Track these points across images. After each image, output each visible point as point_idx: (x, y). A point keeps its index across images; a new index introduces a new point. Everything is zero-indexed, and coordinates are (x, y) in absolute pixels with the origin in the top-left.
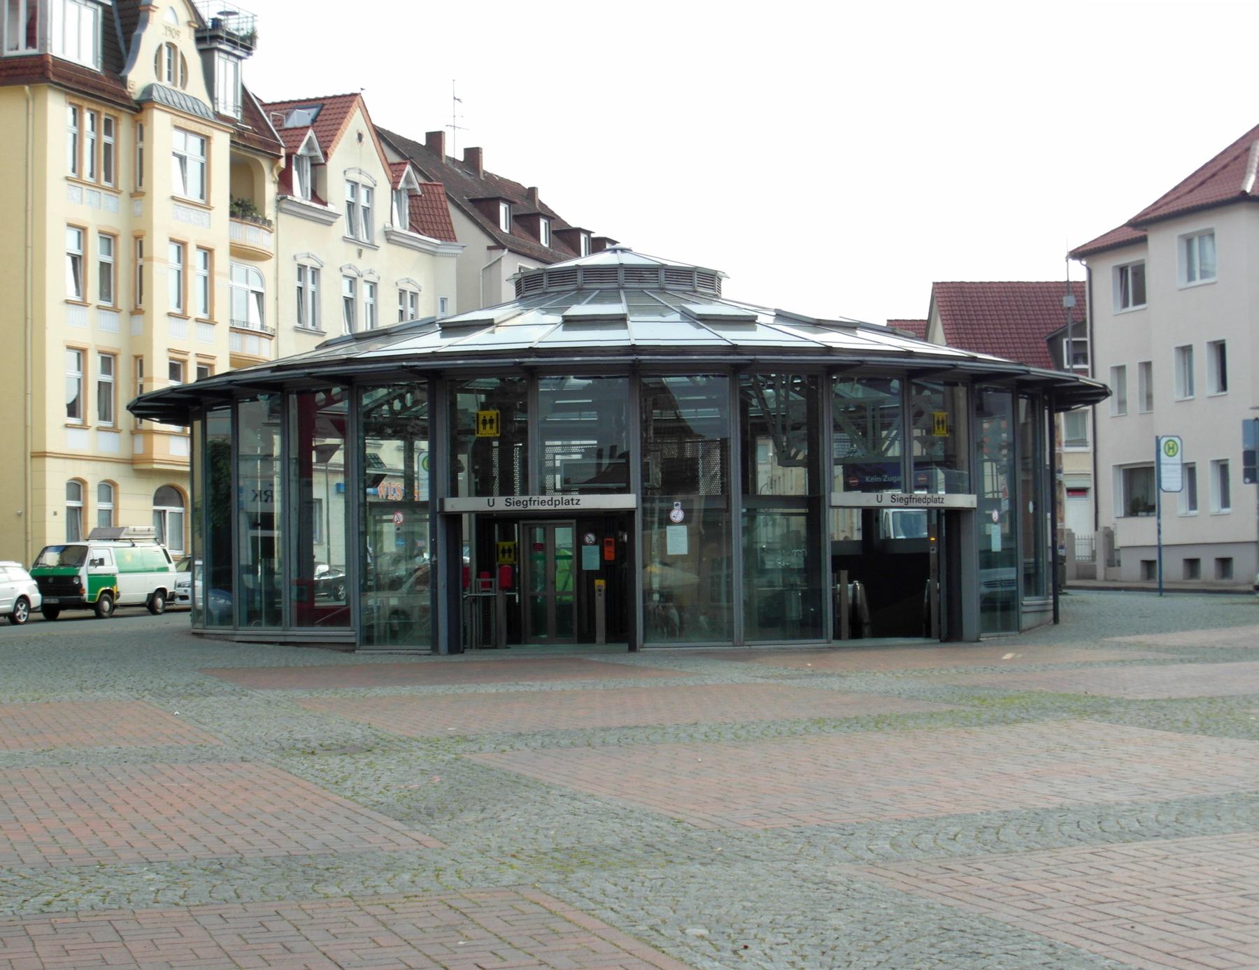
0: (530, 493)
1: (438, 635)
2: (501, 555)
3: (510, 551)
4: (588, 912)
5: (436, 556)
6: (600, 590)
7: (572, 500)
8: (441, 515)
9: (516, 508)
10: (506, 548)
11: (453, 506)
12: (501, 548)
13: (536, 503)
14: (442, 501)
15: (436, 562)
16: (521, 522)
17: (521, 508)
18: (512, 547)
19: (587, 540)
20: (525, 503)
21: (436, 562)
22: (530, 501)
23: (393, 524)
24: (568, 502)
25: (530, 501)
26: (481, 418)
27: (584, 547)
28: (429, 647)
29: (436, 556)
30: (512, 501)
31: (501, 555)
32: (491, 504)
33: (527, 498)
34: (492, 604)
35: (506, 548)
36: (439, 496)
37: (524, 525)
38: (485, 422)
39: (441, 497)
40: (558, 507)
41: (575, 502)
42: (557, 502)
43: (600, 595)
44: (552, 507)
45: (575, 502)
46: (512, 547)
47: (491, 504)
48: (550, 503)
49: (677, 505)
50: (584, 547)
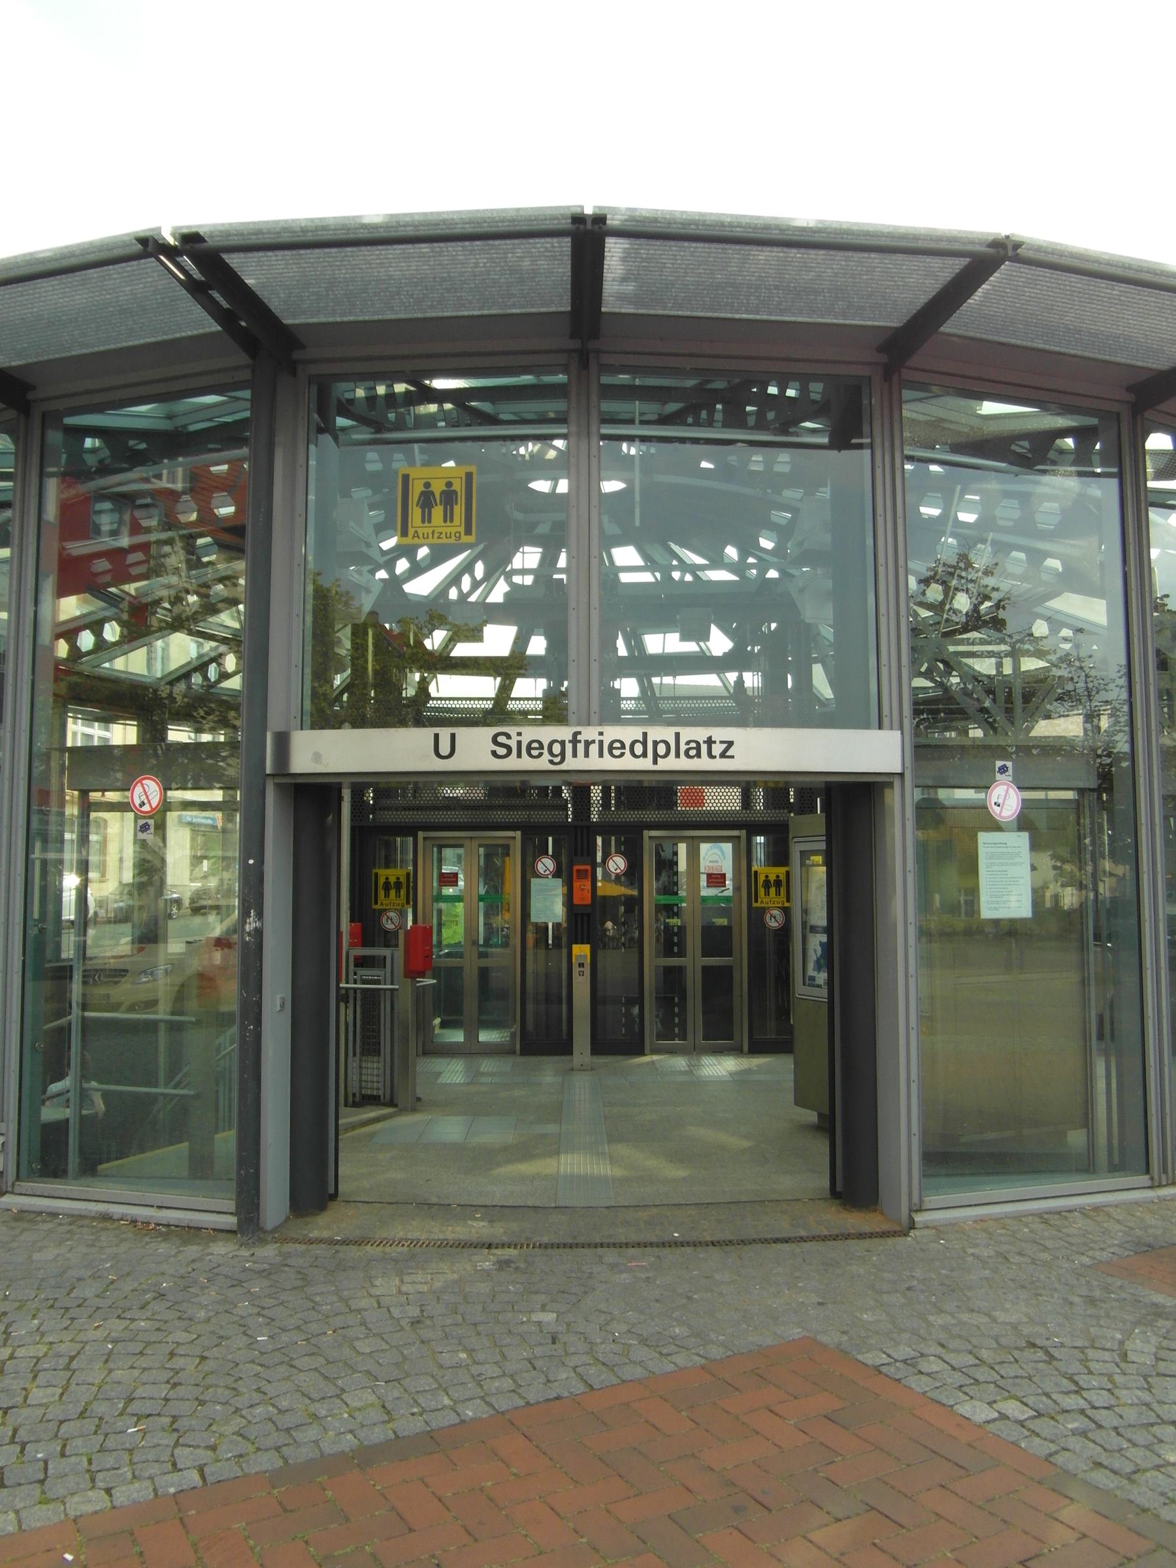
0: (572, 717)
1: (263, 863)
2: (382, 893)
3: (398, 885)
4: (22, 296)
5: (260, 916)
6: (581, 965)
7: (710, 742)
8: (278, 786)
9: (526, 763)
10: (392, 880)
11: (317, 757)
12: (382, 880)
13: (594, 748)
14: (283, 742)
15: (259, 933)
16: (421, 834)
17: (543, 763)
18: (403, 880)
19: (540, 868)
20: (557, 749)
21: (259, 933)
22: (575, 741)
23: (130, 816)
24: (695, 750)
25: (575, 741)
26: (417, 489)
27: (534, 881)
28: (231, 1206)
29: (260, 916)
30: (513, 743)
31: (382, 893)
32: (445, 749)
33: (564, 733)
34: (385, 1007)
35: (772, 878)
36: (275, 723)
37: (425, 839)
38: (427, 500)
39: (281, 728)
40: (664, 765)
41: (717, 749)
42: (661, 749)
43: (582, 974)
44: (646, 764)
45: (717, 749)
46: (403, 880)
47: (445, 749)
48: (639, 749)
49: (1003, 770)
50: (534, 881)
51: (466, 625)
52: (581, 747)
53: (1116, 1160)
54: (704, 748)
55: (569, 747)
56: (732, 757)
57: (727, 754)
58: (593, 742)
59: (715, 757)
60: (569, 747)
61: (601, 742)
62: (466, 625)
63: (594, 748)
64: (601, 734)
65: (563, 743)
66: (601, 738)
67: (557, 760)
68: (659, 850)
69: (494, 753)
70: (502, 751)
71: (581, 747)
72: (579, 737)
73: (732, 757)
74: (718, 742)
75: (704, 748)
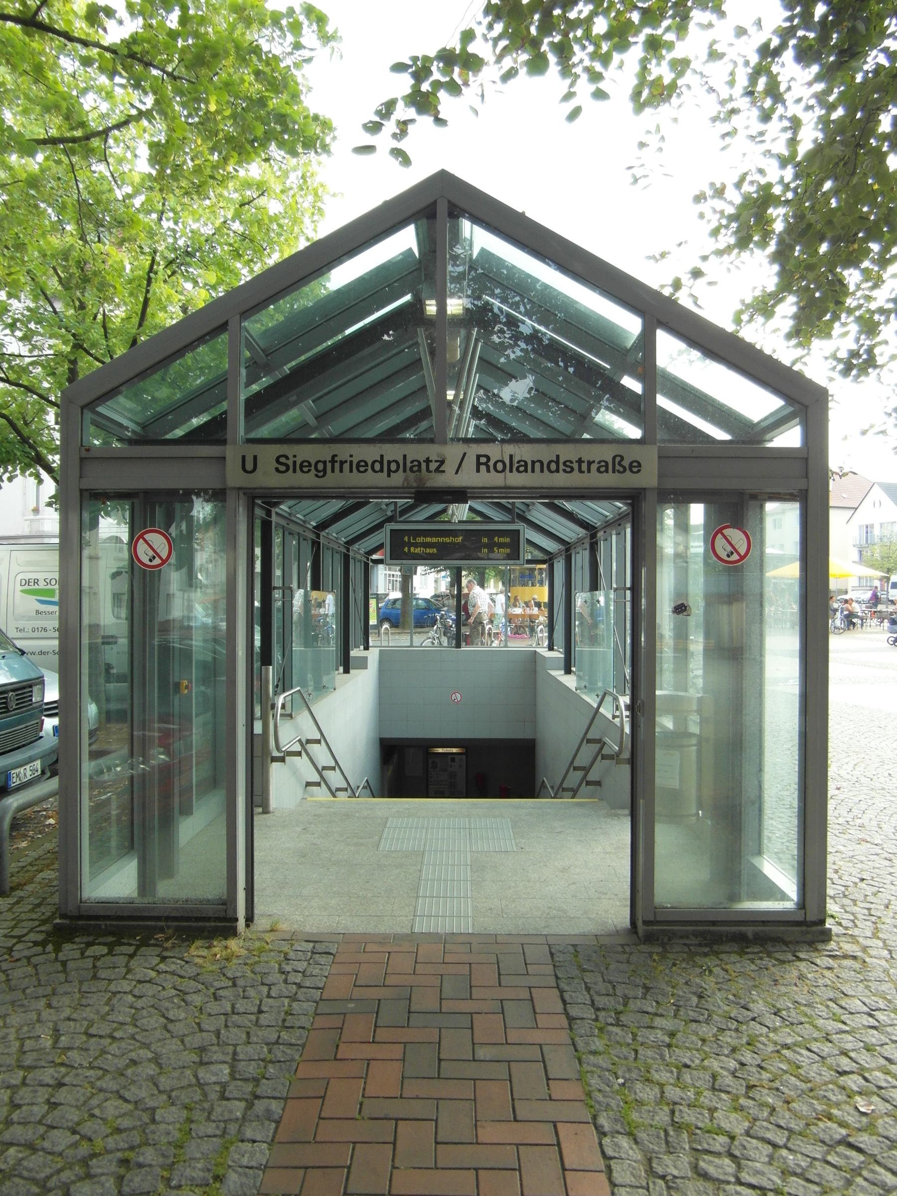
13: (346, 467)
20: (320, 466)
52: (337, 465)
54: (424, 465)
55: (329, 465)
60: (329, 465)
67: (321, 474)
70: (282, 468)
71: (337, 465)
72: (336, 459)
75: (424, 465)
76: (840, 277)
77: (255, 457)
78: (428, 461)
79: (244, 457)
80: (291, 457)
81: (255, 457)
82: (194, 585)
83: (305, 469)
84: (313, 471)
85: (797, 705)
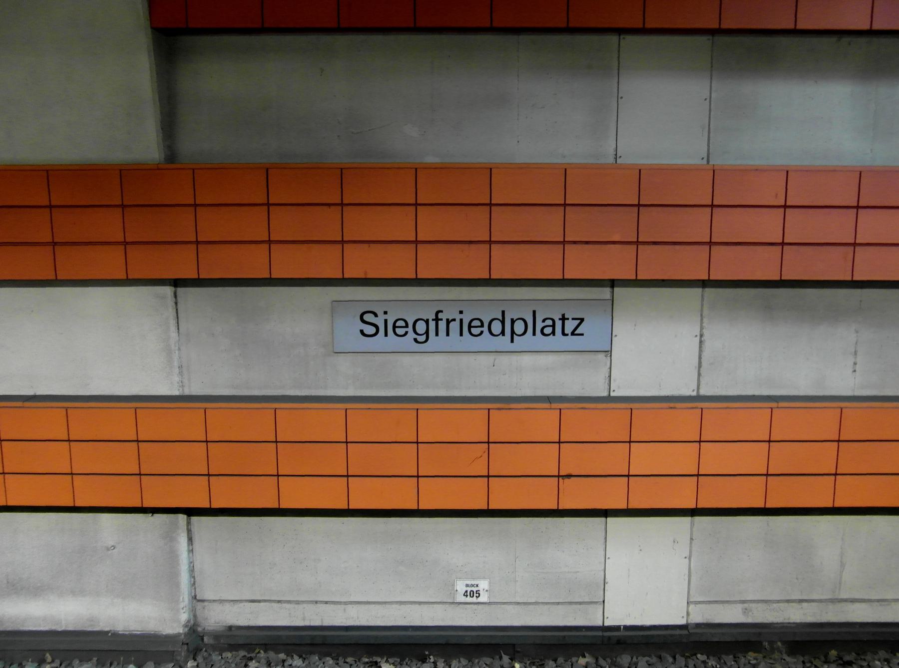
13: (454, 326)
20: (421, 327)
51: (178, 383)
52: (442, 325)
53: (472, 596)
54: (559, 324)
55: (432, 325)
56: (582, 335)
57: (575, 333)
58: (454, 320)
59: (567, 335)
60: (432, 325)
61: (461, 320)
62: (178, 383)
63: (454, 326)
64: (461, 312)
65: (427, 322)
66: (461, 316)
67: (422, 338)
68: (694, 628)
69: (415, 340)
70: (370, 330)
71: (442, 325)
72: (440, 316)
73: (582, 335)
74: (570, 319)
75: (559, 324)
76: (693, 639)
77: (461, 335)
78: (563, 319)
79: (448, 335)
80: (380, 313)
81: (461, 335)
82: (82, 663)
83: (400, 331)
84: (411, 334)
85: (531, 207)
